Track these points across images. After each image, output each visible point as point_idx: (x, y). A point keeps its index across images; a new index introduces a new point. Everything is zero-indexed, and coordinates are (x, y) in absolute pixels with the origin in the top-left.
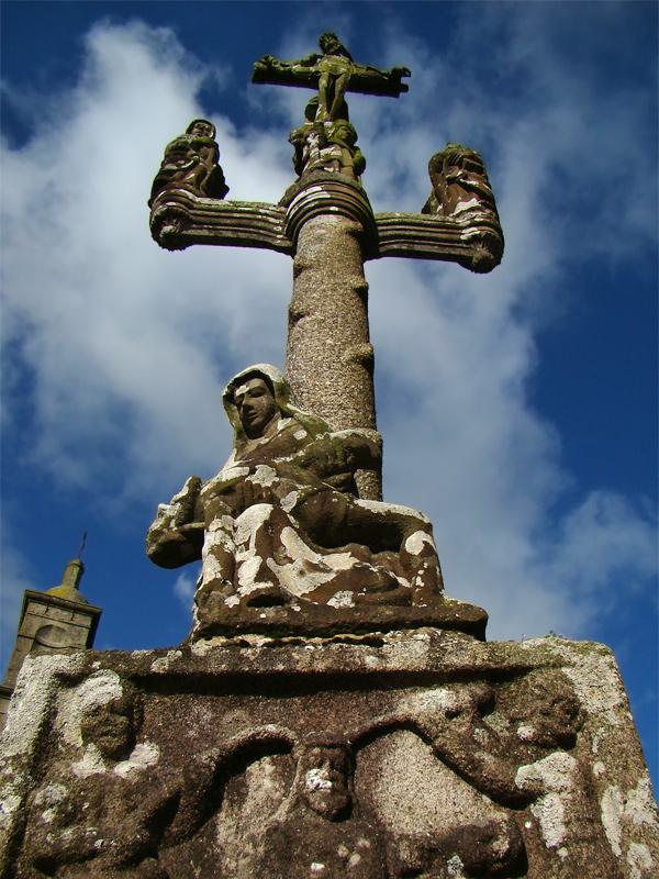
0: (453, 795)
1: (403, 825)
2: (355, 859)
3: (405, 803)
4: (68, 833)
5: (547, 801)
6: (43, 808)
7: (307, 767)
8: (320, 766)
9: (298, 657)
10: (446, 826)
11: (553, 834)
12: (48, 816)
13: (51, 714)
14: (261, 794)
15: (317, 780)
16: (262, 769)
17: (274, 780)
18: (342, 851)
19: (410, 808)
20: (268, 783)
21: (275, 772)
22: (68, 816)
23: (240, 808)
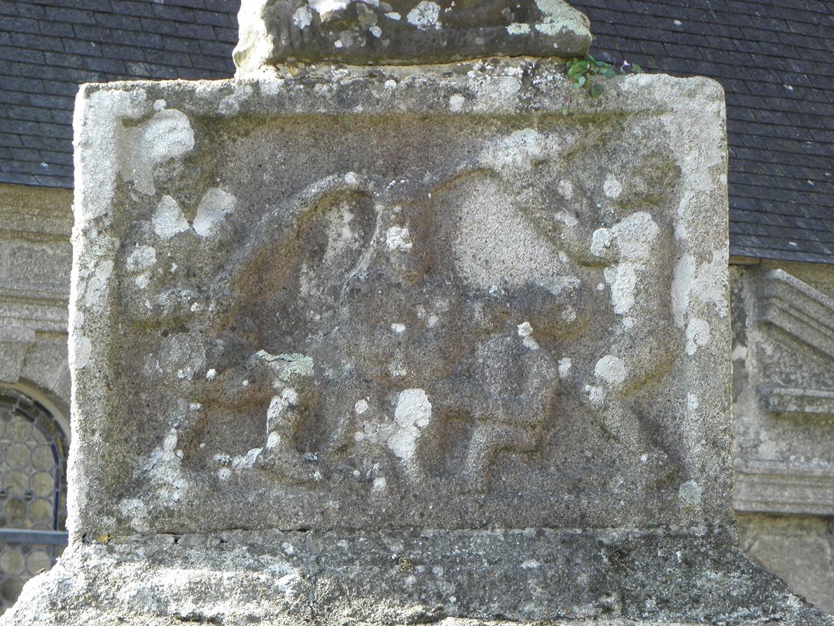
0: (530, 250)
1: (479, 280)
2: (433, 321)
3: (483, 256)
4: (163, 298)
5: (621, 268)
6: (136, 273)
7: (387, 225)
8: (402, 225)
9: (377, 96)
10: (521, 283)
11: (622, 301)
12: (142, 281)
13: (120, 276)
14: (340, 244)
15: (399, 241)
16: (341, 217)
17: (353, 230)
18: (421, 312)
19: (487, 262)
20: (347, 233)
21: (354, 220)
22: (163, 281)
23: (320, 260)
